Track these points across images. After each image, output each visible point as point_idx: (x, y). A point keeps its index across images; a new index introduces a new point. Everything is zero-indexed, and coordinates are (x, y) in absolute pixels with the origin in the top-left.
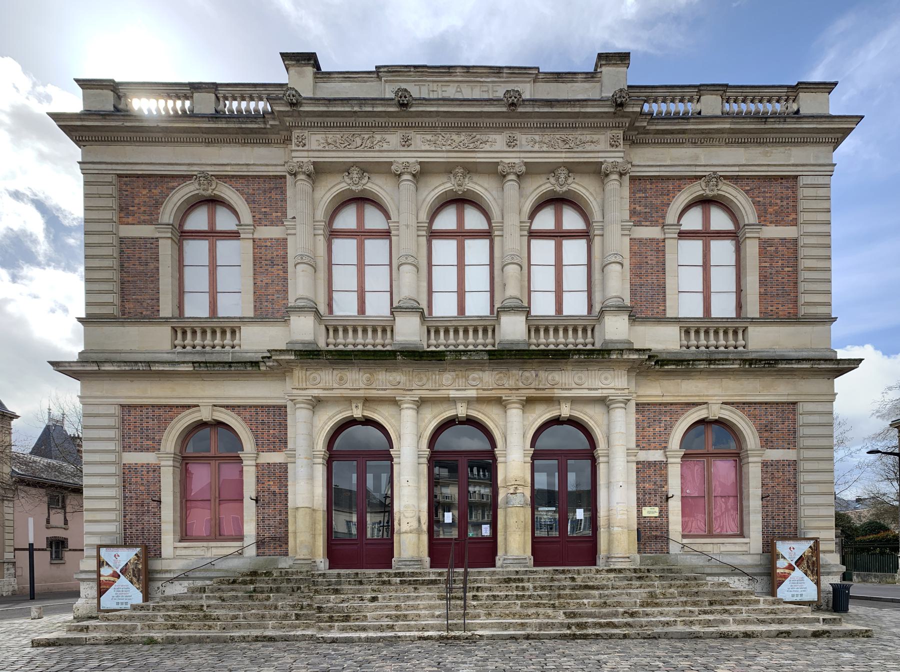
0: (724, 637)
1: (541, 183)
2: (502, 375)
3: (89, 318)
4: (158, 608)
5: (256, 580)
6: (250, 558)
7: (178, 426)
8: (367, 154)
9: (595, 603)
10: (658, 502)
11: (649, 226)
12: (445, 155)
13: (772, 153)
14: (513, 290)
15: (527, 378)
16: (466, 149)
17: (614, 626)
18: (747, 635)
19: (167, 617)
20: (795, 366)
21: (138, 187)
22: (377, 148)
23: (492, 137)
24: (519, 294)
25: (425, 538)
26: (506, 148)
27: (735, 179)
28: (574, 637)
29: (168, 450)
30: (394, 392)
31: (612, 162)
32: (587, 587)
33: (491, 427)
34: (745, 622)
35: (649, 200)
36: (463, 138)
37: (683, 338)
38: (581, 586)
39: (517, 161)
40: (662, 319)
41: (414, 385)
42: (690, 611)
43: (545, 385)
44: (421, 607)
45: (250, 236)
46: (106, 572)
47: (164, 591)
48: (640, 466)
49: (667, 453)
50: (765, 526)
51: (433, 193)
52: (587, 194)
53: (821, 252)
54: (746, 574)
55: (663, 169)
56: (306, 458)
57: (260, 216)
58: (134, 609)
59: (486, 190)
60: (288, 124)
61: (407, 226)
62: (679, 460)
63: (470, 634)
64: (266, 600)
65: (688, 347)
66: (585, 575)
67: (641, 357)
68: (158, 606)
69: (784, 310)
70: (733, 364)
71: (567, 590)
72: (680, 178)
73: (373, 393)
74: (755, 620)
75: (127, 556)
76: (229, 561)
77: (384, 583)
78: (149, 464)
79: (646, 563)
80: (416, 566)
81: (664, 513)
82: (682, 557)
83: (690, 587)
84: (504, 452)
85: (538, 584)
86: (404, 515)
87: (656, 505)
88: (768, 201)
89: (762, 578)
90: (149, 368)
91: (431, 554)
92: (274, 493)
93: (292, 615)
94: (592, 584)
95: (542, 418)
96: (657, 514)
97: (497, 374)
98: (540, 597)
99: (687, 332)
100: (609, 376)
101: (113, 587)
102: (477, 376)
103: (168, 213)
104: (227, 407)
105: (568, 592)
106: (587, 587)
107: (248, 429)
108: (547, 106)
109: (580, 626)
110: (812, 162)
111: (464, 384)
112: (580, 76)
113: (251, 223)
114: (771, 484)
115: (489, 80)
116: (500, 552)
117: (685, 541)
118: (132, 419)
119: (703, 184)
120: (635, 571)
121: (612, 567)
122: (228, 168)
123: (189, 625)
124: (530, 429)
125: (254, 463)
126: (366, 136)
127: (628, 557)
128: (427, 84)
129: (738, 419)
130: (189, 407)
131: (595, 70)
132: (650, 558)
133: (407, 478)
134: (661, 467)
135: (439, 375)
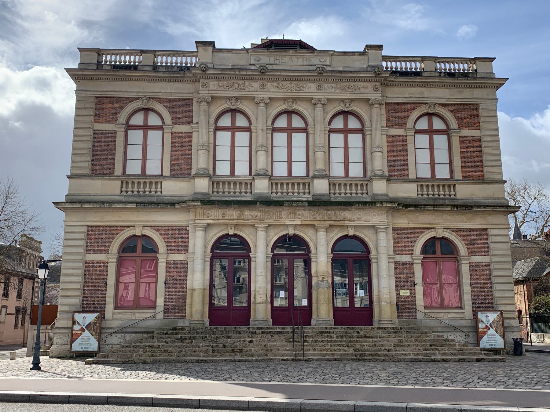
0: (433, 361)
1: (335, 106)
2: (315, 213)
3: (72, 176)
4: (136, 347)
5: (179, 332)
6: (160, 320)
7: (121, 238)
8: (241, 93)
9: (369, 345)
10: (409, 287)
11: (398, 128)
12: (283, 94)
13: (463, 92)
14: (320, 165)
15: (330, 215)
16: (295, 91)
17: (379, 356)
18: (444, 360)
19: (145, 351)
20: (483, 209)
21: (106, 103)
22: (247, 89)
23: (309, 84)
24: (324, 167)
25: (269, 306)
26: (316, 91)
27: (444, 105)
28: (359, 360)
29: (113, 252)
30: (253, 221)
31: (375, 99)
32: (365, 337)
33: (308, 241)
34: (445, 354)
35: (397, 114)
36: (293, 85)
37: (419, 190)
38: (362, 336)
39: (322, 97)
40: (406, 179)
41: (266, 217)
42: (419, 349)
43: (340, 219)
44: (278, 345)
45: (170, 131)
46: (77, 327)
47: (106, 341)
48: (397, 264)
49: (413, 257)
50: (474, 303)
51: (275, 111)
52: (362, 112)
53: (494, 145)
54: (463, 331)
55: (404, 99)
56: (201, 259)
57: (176, 120)
58: (123, 347)
59: (305, 109)
60: (198, 77)
61: (262, 130)
62: (420, 261)
63: (307, 358)
64: (190, 343)
65: (422, 195)
66: (365, 331)
67: (393, 206)
68: (136, 346)
69: (476, 175)
70: (447, 208)
71: (355, 338)
72: (133, 98)
73: (242, 222)
74: (450, 354)
75: (91, 317)
76: (147, 321)
77: (253, 333)
78: (101, 261)
79: (403, 325)
80: (266, 324)
81: (413, 294)
82: (424, 321)
83: (422, 337)
84: (316, 256)
85: (339, 335)
86: (259, 293)
87: (408, 289)
88: (463, 116)
89: (473, 334)
90: (110, 206)
91: (272, 317)
92: (176, 279)
93: (210, 350)
94: (368, 335)
95: (337, 236)
96: (408, 294)
97: (313, 212)
98: (340, 341)
99: (422, 186)
100: (376, 214)
101: (80, 337)
102: (301, 213)
103: (122, 118)
104: (150, 227)
105: (355, 339)
106: (365, 337)
107: (163, 240)
108: (339, 73)
109: (361, 355)
110: (485, 97)
111: (294, 218)
112: (357, 54)
113: (171, 124)
114: (476, 277)
115: (307, 55)
116: (314, 316)
117: (426, 311)
118: (93, 233)
119: (427, 107)
120: (393, 328)
121: (381, 326)
122: (160, 94)
123: (160, 355)
124: (330, 242)
125: (165, 260)
126: (241, 83)
127: (391, 321)
128: (273, 56)
129: (454, 237)
130: (128, 227)
131: (365, 50)
132: (406, 321)
133: (261, 271)
134: (410, 265)
135: (279, 212)
